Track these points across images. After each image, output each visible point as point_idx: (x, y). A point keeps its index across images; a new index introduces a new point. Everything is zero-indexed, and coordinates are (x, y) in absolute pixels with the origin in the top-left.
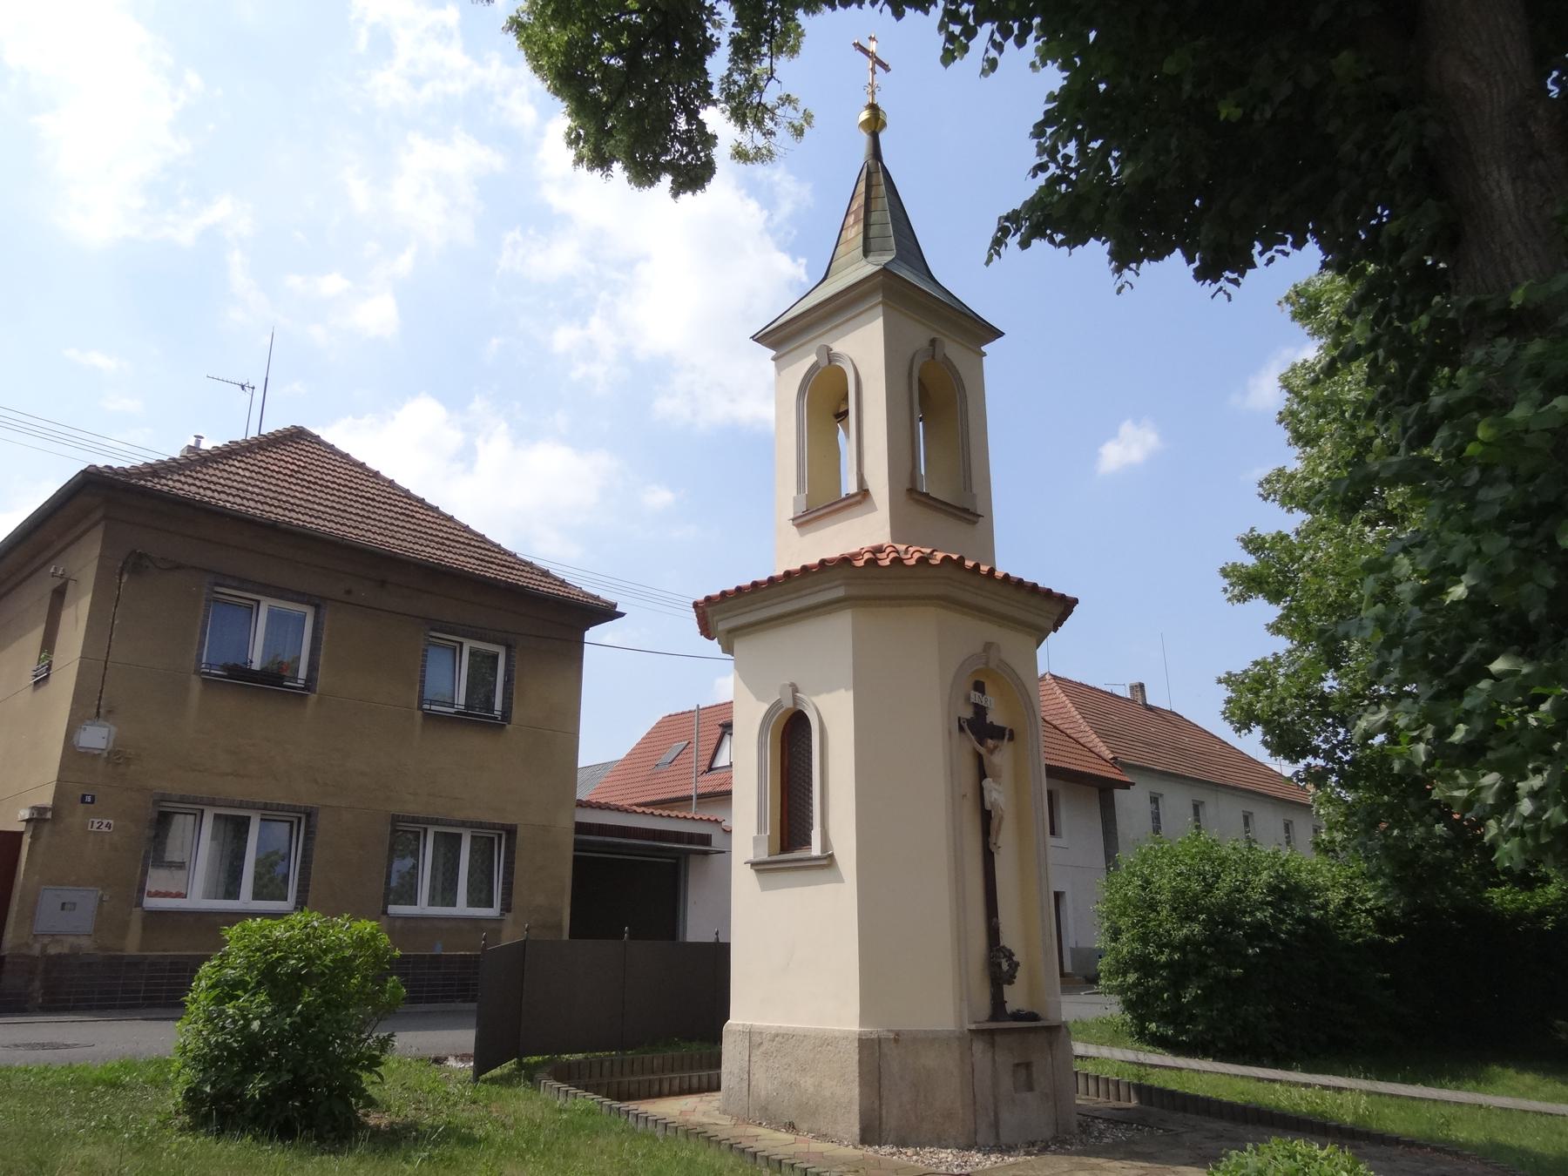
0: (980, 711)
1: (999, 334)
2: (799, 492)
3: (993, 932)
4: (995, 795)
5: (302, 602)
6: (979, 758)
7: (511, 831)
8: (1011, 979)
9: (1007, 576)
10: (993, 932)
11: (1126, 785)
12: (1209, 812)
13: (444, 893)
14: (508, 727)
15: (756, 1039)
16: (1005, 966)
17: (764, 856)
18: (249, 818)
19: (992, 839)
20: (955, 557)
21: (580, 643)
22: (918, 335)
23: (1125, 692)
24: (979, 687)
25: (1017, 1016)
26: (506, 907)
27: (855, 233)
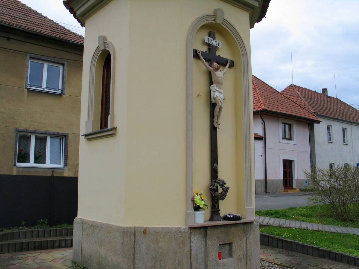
0: (212, 48)
3: (214, 173)
4: (217, 94)
6: (210, 74)
8: (223, 196)
10: (214, 173)
11: (318, 122)
12: (348, 132)
13: (40, 158)
14: (64, 96)
15: (85, 226)
16: (220, 190)
23: (320, 92)
25: (226, 218)
26: (66, 164)
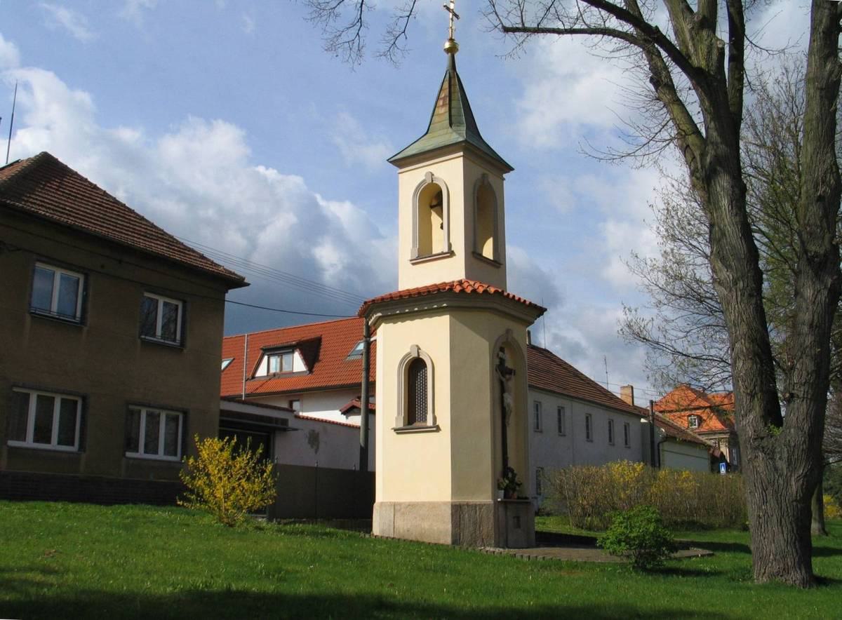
0: (502, 361)
1: (512, 169)
2: (413, 247)
5: (78, 272)
6: (502, 383)
7: (185, 413)
9: (530, 303)
13: (151, 447)
15: (398, 508)
17: (401, 425)
18: (54, 398)
19: (507, 421)
20: (500, 291)
21: (222, 301)
22: (478, 171)
24: (502, 350)
27: (443, 110)
